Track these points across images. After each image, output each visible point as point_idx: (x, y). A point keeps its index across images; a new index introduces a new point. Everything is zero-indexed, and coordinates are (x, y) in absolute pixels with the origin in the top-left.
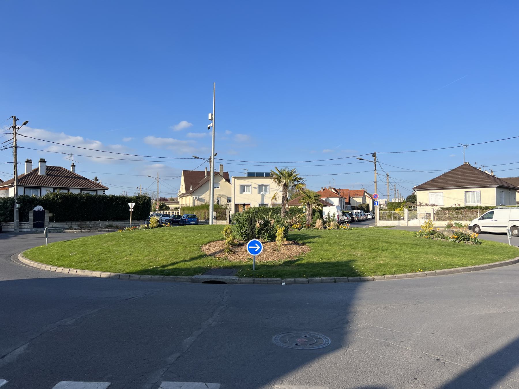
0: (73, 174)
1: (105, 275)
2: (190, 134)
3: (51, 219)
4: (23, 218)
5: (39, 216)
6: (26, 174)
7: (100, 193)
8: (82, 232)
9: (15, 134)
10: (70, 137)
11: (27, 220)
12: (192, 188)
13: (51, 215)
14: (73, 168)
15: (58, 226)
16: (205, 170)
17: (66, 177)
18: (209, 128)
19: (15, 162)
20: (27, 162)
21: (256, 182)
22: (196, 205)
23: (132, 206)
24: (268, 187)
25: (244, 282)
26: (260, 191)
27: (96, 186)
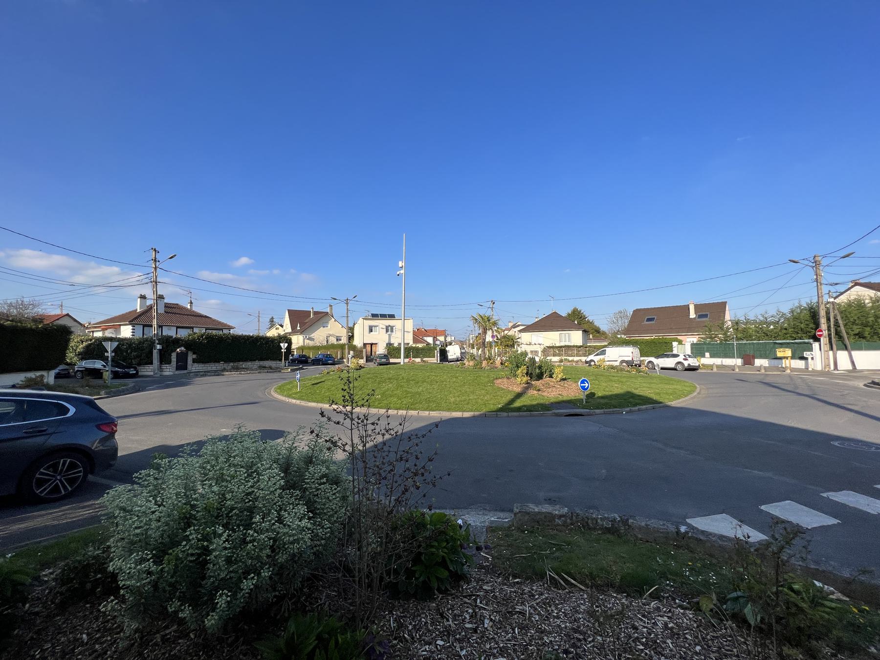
0: (190, 310)
1: (467, 415)
2: (252, 271)
3: (194, 361)
4: (164, 358)
5: (182, 359)
6: (138, 311)
7: (225, 331)
8: (241, 374)
9: (156, 268)
10: (103, 267)
11: (169, 362)
12: (300, 327)
13: (194, 356)
14: (190, 305)
15: (201, 368)
16: (311, 310)
17: (188, 315)
18: (398, 275)
19: (155, 298)
20: (140, 298)
21: (382, 323)
22: (330, 343)
23: (284, 347)
24: (394, 328)
25: (598, 413)
26: (387, 331)
27: (223, 326)
